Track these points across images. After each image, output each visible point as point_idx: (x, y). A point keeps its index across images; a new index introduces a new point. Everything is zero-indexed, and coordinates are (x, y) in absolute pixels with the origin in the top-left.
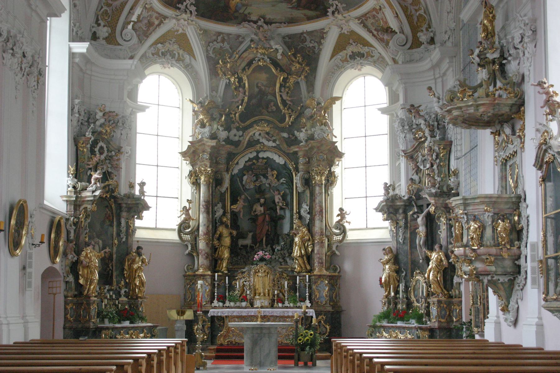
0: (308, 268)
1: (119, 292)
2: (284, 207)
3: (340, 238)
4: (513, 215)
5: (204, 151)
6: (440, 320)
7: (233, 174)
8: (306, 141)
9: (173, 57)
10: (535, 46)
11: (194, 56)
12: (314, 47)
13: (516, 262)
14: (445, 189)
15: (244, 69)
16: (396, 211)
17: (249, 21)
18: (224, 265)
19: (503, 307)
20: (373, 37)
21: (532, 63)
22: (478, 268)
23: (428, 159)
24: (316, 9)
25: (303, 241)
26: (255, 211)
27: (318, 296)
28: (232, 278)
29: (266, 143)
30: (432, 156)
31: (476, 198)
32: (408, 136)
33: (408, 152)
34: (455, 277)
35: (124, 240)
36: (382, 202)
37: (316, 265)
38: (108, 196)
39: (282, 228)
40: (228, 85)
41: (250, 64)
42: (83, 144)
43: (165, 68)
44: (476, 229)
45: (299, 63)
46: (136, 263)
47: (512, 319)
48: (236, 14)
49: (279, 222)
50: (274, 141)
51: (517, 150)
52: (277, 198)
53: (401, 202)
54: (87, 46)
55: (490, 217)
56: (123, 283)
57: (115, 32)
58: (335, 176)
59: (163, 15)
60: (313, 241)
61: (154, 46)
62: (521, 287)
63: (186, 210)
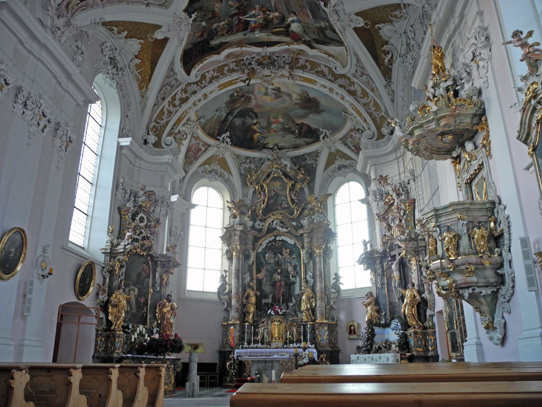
0: (313, 318)
1: (152, 331)
2: (295, 275)
3: (336, 295)
4: (488, 222)
5: (235, 235)
6: (417, 349)
7: (258, 252)
8: (308, 225)
9: (217, 174)
10: (490, 51)
11: (231, 174)
12: (313, 164)
13: (499, 271)
14: (413, 236)
15: (265, 180)
16: (374, 263)
17: (267, 148)
18: (251, 317)
19: (488, 324)
20: (352, 152)
21: (490, 68)
22: (457, 281)
23: (397, 216)
24: (311, 137)
25: (309, 299)
26: (275, 279)
27: (320, 339)
28: (256, 327)
29: (281, 229)
30: (400, 213)
31: (447, 207)
32: (380, 203)
33: (380, 215)
34: (428, 309)
35: (158, 289)
36: (362, 255)
37: (318, 315)
38: (145, 254)
39: (294, 292)
40: (254, 192)
41: (268, 176)
42: (124, 212)
43: (211, 181)
44: (451, 239)
45: (302, 174)
46: (166, 308)
47: (499, 335)
48: (258, 144)
49: (292, 286)
50: (287, 228)
51: (482, 163)
52: (290, 269)
53: (377, 254)
54: (131, 140)
55: (464, 226)
56: (155, 323)
57: (161, 141)
58: (330, 250)
59: (207, 144)
60: (316, 298)
61: (203, 166)
62: (507, 298)
63: (223, 278)
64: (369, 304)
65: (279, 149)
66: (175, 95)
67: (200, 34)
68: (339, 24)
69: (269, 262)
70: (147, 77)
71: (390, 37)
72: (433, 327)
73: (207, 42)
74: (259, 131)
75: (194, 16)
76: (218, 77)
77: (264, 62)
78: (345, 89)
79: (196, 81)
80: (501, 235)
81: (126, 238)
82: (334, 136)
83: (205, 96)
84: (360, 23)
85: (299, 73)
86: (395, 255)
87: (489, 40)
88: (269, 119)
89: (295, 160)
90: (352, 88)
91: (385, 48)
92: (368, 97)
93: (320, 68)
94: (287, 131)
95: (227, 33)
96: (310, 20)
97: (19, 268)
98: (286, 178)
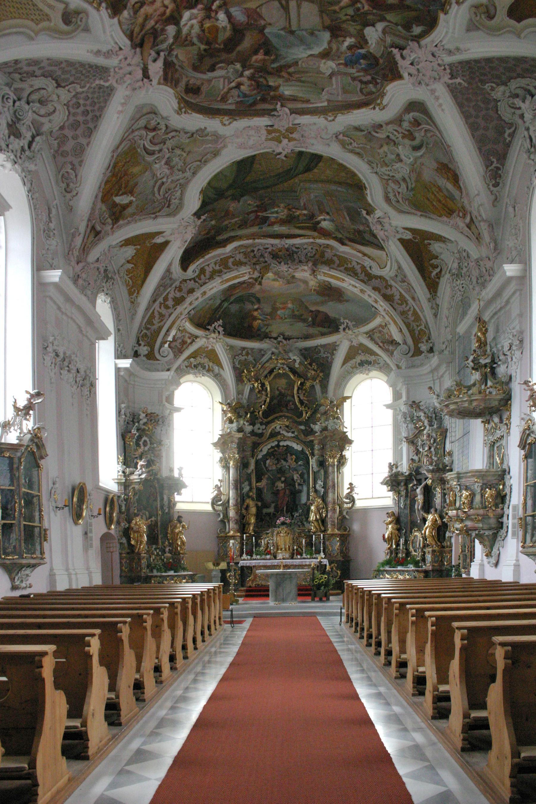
0: (323, 529)
3: (350, 505)
12: (327, 357)
14: (441, 466)
15: (266, 376)
16: (398, 484)
17: (270, 338)
25: (318, 509)
28: (258, 538)
32: (409, 425)
36: (387, 477)
39: (300, 500)
45: (314, 370)
49: (297, 495)
50: (293, 432)
56: (167, 543)
63: (218, 488)
64: (390, 523)
65: (285, 339)
66: (168, 294)
67: (206, 231)
68: (382, 233)
69: (270, 469)
70: (140, 282)
71: (441, 253)
72: (451, 546)
73: (214, 238)
74: (260, 317)
75: (203, 217)
76: (220, 272)
77: (280, 253)
78: (379, 292)
79: (193, 277)
80: (505, 495)
81: (139, 467)
82: (358, 328)
83: (204, 293)
84: (408, 236)
85: (325, 269)
86: (421, 480)
87: (522, 344)
88: (275, 304)
89: (306, 353)
90: (389, 292)
91: (434, 262)
92: (407, 304)
93: (351, 264)
94: (297, 318)
95: (239, 227)
96: (347, 222)
97: (84, 514)
98: (294, 376)
